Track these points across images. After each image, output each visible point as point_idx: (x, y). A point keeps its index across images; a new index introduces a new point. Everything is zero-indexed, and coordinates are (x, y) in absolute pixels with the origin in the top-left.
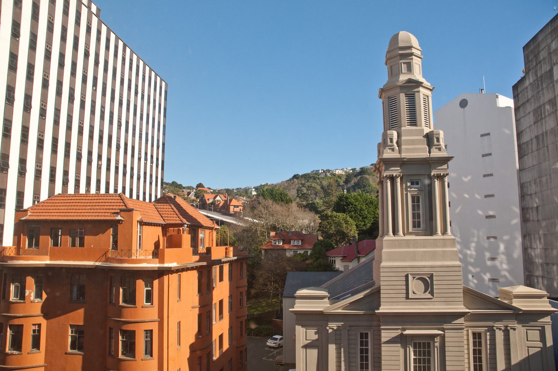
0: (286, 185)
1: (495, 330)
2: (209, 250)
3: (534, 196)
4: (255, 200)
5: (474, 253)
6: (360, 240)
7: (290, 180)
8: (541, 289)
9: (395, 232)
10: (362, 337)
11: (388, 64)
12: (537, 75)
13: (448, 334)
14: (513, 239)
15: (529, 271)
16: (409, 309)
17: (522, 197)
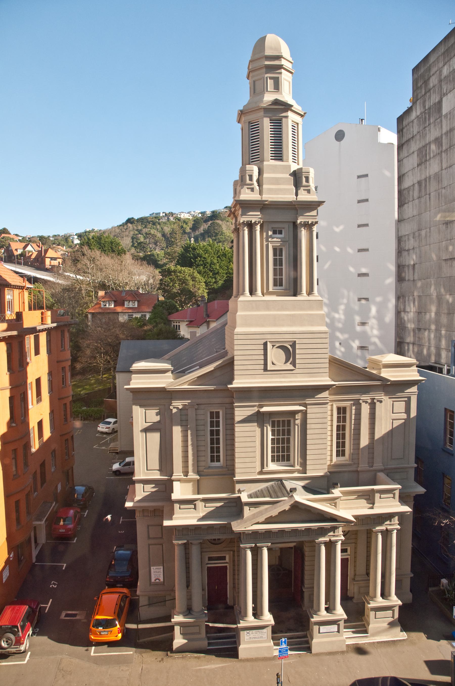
0: (118, 231)
1: (361, 404)
2: (19, 315)
3: (411, 252)
4: (78, 251)
5: (342, 317)
6: (210, 300)
7: (123, 225)
8: (411, 357)
9: (252, 292)
10: (212, 417)
11: (250, 78)
12: (424, 107)
13: (311, 410)
14: (386, 301)
15: (401, 338)
16: (266, 382)
17: (398, 252)
